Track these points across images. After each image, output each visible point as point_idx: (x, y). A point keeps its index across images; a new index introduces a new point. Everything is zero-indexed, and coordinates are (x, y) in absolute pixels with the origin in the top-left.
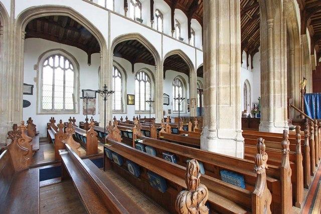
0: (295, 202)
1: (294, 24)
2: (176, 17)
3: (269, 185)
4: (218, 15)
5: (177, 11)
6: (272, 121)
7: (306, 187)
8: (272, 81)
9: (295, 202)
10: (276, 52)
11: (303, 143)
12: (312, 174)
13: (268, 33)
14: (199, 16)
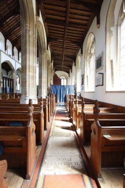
0: (51, 116)
1: (49, 58)
2: (14, 50)
3: (35, 122)
4: (29, 53)
5: (8, 41)
6: (42, 94)
7: (52, 112)
8: (42, 79)
9: (51, 116)
10: (31, 45)
11: (45, 106)
12: (45, 129)
13: (41, 60)
14: (3, 31)
